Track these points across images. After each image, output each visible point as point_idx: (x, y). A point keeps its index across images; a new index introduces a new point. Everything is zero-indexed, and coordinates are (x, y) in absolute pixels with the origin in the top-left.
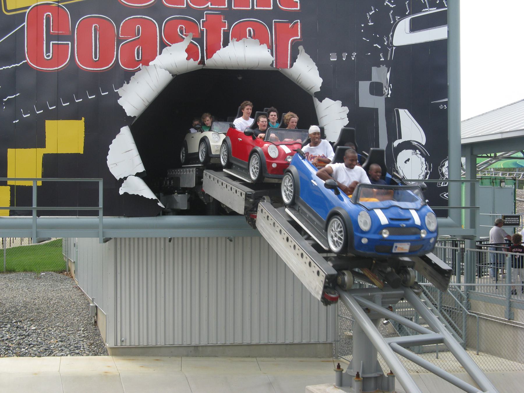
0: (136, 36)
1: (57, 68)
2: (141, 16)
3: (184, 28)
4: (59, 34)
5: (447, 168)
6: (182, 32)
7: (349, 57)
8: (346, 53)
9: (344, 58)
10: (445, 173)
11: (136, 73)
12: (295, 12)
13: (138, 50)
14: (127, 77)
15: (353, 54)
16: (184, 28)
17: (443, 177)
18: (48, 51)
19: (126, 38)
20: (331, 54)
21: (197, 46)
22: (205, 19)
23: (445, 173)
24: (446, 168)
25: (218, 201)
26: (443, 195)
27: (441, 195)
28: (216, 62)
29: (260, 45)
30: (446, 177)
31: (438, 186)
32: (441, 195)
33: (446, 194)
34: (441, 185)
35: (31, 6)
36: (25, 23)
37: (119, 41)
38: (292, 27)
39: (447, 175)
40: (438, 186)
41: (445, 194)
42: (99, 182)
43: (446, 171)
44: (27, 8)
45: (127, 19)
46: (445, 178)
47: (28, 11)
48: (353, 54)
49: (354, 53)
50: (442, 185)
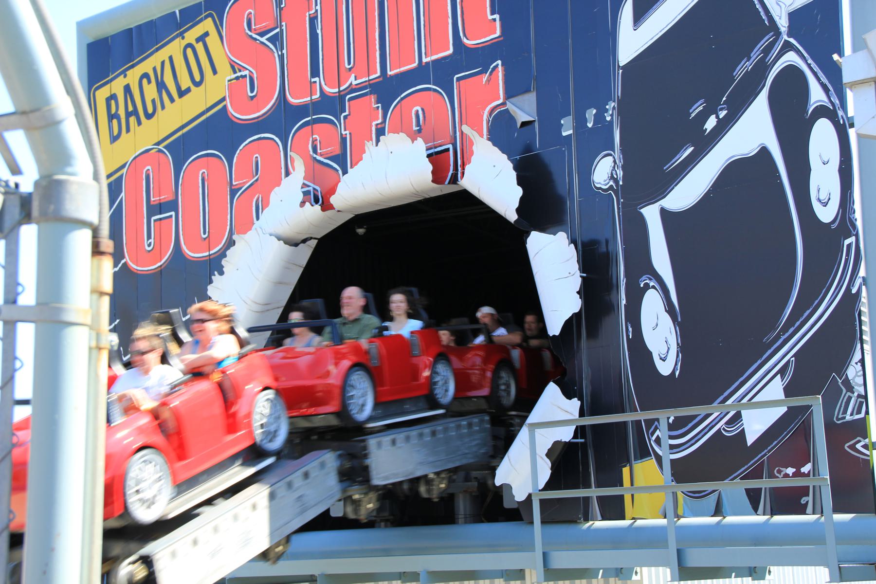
0: (254, 177)
1: (159, 264)
2: (399, 98)
3: (318, 139)
4: (162, 201)
5: (859, 364)
6: (315, 150)
7: (580, 122)
8: (593, 109)
9: (590, 123)
10: (854, 379)
11: (228, 253)
12: (493, 43)
13: (257, 202)
14: (214, 265)
15: (607, 107)
16: (318, 139)
17: (849, 394)
18: (149, 237)
19: (240, 184)
20: (562, 122)
21: (337, 170)
22: (347, 113)
23: (854, 381)
24: (856, 363)
25: (191, 520)
26: (853, 447)
27: (848, 447)
28: (345, 199)
29: (413, 142)
30: (858, 391)
31: (838, 419)
32: (848, 447)
33: (862, 443)
34: (844, 418)
35: (127, 162)
36: (123, 194)
37: (233, 193)
38: (489, 80)
39: (859, 385)
40: (838, 419)
41: (859, 441)
42: (579, 417)
43: (856, 375)
44: (123, 166)
45: (241, 148)
46: (856, 394)
47: (125, 170)
48: (607, 107)
49: (609, 103)
50: (848, 418)
